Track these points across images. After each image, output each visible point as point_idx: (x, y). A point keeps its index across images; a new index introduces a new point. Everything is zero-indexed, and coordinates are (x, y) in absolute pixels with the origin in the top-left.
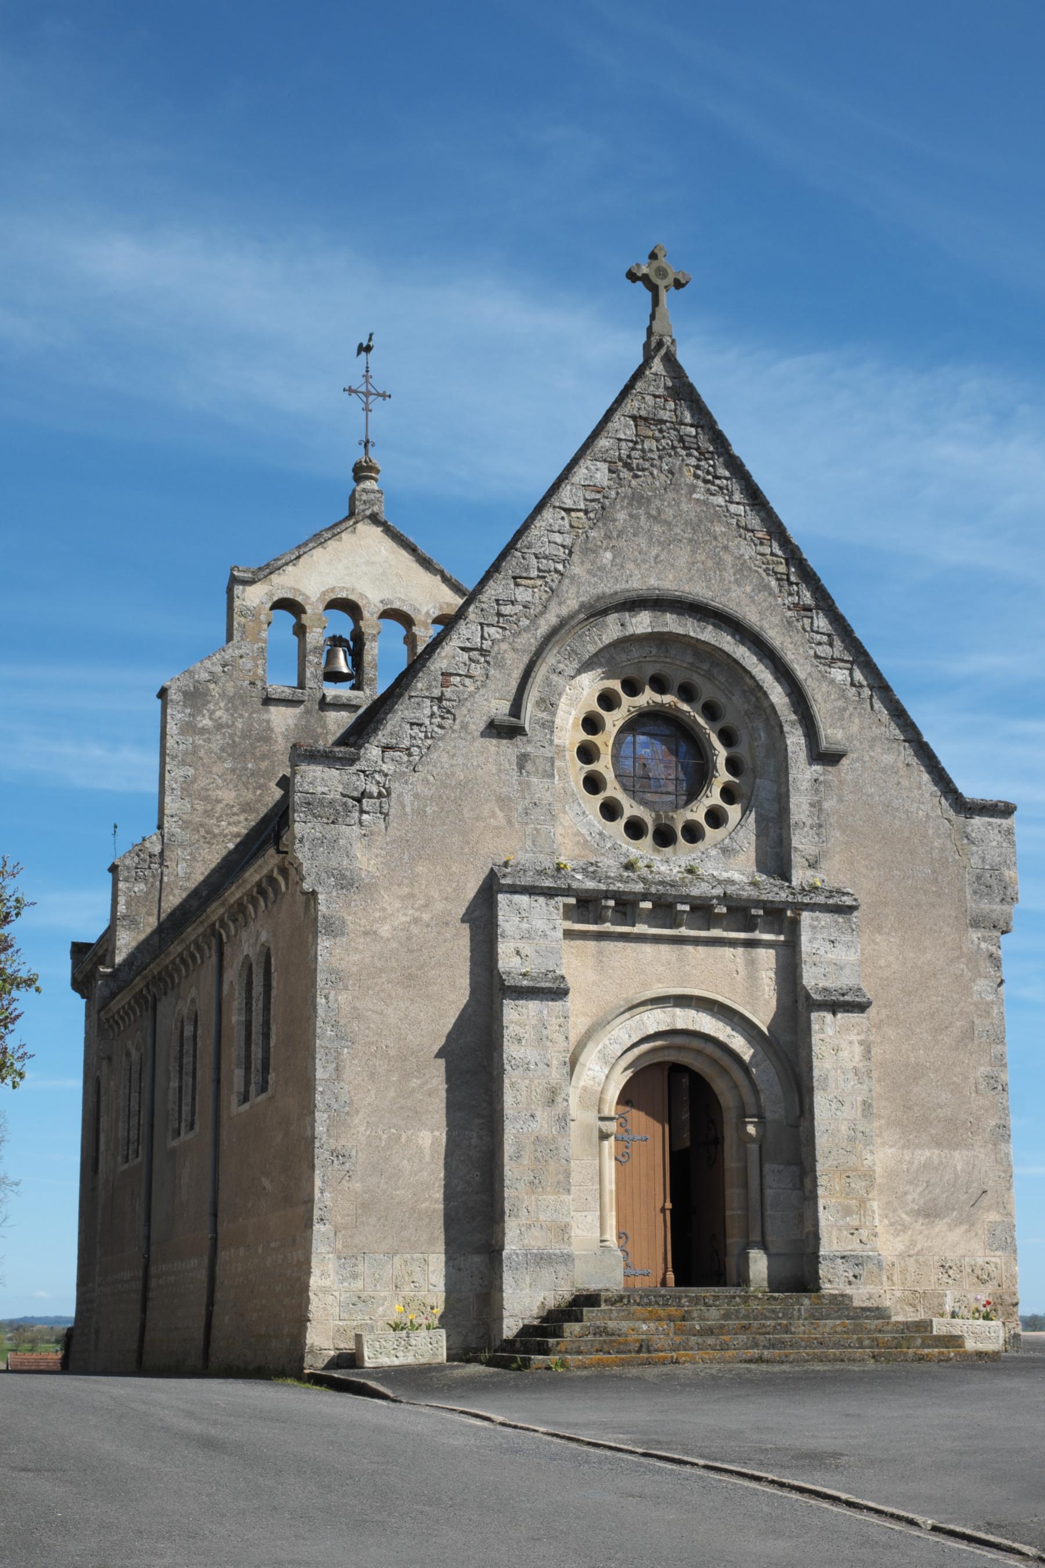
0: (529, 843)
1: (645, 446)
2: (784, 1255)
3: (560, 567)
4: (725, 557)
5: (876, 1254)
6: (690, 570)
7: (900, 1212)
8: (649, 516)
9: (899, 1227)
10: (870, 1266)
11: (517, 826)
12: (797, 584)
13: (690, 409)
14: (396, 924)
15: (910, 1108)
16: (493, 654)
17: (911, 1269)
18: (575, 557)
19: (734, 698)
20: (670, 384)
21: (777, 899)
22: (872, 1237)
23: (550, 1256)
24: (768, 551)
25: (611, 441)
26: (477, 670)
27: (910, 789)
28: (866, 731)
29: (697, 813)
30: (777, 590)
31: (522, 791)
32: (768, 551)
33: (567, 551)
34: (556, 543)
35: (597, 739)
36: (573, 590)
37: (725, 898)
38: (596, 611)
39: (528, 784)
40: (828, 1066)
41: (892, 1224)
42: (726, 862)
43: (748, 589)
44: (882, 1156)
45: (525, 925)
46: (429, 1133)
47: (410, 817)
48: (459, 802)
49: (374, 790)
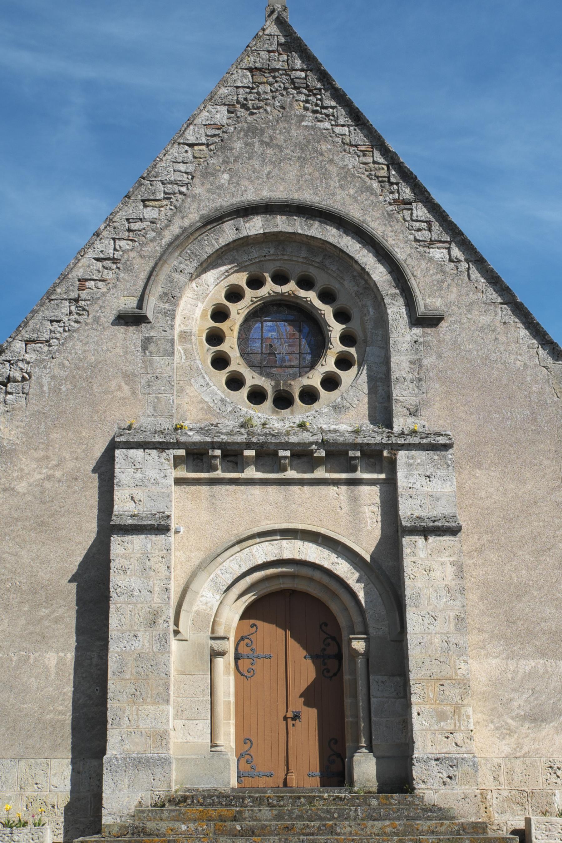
0: (151, 409)
1: (260, 90)
2: (388, 757)
3: (184, 189)
4: (331, 169)
5: (471, 756)
6: (298, 181)
7: (505, 717)
8: (262, 143)
9: (505, 731)
10: (465, 767)
11: (140, 396)
12: (397, 184)
13: (301, 57)
14: (31, 481)
15: (514, 623)
16: (123, 261)
17: (518, 770)
18: (197, 181)
19: (346, 283)
20: (282, 40)
21: (372, 441)
22: (467, 740)
23: (148, 760)
24: (370, 160)
25: (230, 89)
26: (109, 275)
27: (508, 344)
28: (464, 298)
29: (314, 379)
30: (379, 191)
31: (146, 367)
32: (370, 160)
33: (190, 177)
34: (180, 171)
35: (224, 326)
36: (195, 205)
37: (323, 444)
38: (214, 220)
39: (151, 362)
40: (420, 585)
41: (497, 729)
42: (342, 415)
43: (352, 191)
44: (481, 668)
45: (139, 475)
46: (55, 654)
47: (47, 395)
48: (90, 380)
49: (18, 375)
